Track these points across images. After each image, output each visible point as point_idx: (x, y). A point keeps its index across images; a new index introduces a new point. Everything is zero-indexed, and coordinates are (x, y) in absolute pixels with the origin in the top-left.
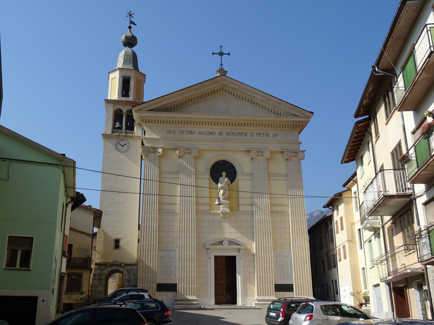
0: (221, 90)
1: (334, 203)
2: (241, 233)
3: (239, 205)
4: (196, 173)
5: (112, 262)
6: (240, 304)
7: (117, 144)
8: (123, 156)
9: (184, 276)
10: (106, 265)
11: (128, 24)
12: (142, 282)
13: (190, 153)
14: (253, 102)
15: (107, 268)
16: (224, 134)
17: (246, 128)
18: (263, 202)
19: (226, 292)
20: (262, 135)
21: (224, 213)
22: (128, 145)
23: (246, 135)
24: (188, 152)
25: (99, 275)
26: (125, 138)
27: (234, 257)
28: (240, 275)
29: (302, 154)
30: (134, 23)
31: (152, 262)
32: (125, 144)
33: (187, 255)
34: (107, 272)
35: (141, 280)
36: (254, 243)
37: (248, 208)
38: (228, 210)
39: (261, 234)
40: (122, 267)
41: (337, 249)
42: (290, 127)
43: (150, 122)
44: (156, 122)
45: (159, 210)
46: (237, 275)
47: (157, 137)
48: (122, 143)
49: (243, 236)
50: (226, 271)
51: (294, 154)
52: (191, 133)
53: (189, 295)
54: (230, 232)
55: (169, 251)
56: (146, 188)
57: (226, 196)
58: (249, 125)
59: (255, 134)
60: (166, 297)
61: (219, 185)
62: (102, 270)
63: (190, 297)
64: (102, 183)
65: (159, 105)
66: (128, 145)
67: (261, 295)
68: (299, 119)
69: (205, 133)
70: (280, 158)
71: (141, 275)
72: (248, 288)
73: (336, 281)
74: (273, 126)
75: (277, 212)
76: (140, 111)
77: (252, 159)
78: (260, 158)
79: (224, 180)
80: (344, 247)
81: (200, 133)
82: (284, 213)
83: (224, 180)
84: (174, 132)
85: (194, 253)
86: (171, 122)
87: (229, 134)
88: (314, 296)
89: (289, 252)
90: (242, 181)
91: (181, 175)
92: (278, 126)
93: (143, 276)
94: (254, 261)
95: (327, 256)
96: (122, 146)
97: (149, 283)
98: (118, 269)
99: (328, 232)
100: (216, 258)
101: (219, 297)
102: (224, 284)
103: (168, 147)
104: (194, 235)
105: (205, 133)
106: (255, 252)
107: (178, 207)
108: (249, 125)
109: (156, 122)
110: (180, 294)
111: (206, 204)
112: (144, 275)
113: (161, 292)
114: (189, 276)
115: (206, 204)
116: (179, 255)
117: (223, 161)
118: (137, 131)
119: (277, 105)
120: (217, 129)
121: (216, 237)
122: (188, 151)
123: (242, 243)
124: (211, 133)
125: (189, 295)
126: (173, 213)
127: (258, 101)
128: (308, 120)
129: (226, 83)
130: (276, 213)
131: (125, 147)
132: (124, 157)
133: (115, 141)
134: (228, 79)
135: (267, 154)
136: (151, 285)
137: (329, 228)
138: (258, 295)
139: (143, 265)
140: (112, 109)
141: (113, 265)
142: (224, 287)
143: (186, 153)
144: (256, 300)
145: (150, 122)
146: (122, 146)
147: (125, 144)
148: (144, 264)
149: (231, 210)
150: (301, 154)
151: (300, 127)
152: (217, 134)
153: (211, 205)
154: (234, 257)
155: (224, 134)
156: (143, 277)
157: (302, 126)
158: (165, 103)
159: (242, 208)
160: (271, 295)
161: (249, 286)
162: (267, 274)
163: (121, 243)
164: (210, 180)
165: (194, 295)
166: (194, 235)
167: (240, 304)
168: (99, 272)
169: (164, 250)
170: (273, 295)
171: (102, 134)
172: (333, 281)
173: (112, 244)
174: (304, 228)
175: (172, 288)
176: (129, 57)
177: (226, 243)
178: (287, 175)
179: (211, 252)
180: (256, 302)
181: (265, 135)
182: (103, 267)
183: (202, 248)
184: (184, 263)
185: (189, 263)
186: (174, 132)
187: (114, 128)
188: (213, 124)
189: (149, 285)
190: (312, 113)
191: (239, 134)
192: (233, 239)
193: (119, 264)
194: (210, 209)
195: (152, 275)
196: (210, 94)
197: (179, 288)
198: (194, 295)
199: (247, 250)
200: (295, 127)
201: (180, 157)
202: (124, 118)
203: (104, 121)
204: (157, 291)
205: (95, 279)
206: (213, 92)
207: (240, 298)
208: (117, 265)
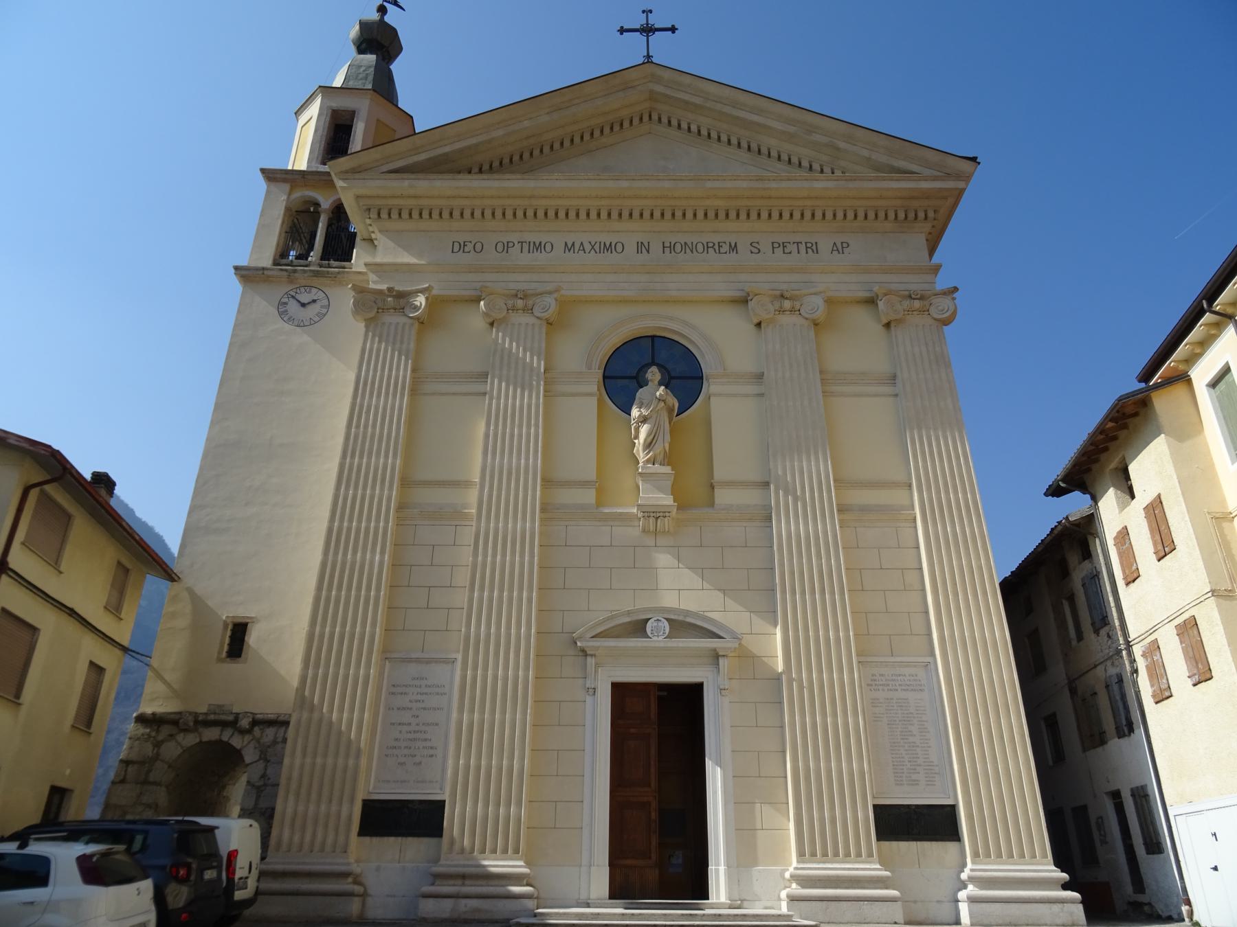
0: (646, 118)
1: (1098, 461)
2: (724, 591)
3: (712, 487)
4: (550, 377)
5: (203, 709)
6: (723, 898)
8: (301, 338)
9: (478, 768)
10: (175, 723)
12: (298, 794)
13: (529, 310)
14: (754, 146)
15: (180, 737)
16: (656, 248)
17: (732, 225)
18: (813, 472)
19: (661, 841)
20: (789, 248)
21: (654, 514)
22: (325, 302)
23: (734, 248)
24: (520, 303)
25: (141, 763)
27: (695, 691)
29: (945, 302)
31: (356, 715)
32: (314, 301)
33: (495, 677)
34: (179, 751)
35: (294, 786)
36: (778, 631)
37: (749, 497)
38: (667, 500)
39: (803, 593)
40: (243, 732)
41: (1137, 650)
42: (891, 215)
43: (395, 215)
44: (415, 214)
45: (401, 507)
47: (413, 260)
48: (305, 298)
52: (539, 247)
53: (494, 851)
54: (678, 587)
55: (428, 661)
56: (358, 427)
57: (659, 448)
59: (765, 247)
60: (387, 867)
62: (158, 745)
63: (496, 865)
65: (423, 157)
66: (325, 302)
67: (814, 854)
68: (925, 185)
69: (588, 247)
71: (298, 762)
73: (1142, 796)
75: (864, 509)
76: (357, 176)
77: (759, 325)
78: (786, 319)
79: (655, 391)
80: (1189, 630)
81: (569, 248)
82: (898, 516)
83: (655, 391)
84: (478, 247)
85: (527, 668)
86: (467, 213)
87: (672, 248)
88: (1060, 862)
89: (927, 665)
90: (726, 408)
91: (494, 385)
92: (850, 215)
93: (335, 766)
94: (781, 703)
95: (1073, 691)
96: (303, 305)
97: (314, 796)
98: (225, 738)
99: (1071, 599)
101: (628, 862)
102: (654, 805)
103: (455, 293)
107: (473, 496)
109: (415, 214)
110: (457, 847)
111: (584, 484)
112: (308, 760)
113: (375, 840)
114: (500, 769)
115: (584, 484)
116: (464, 677)
120: (629, 233)
121: (624, 604)
122: (523, 300)
123: (722, 626)
124: (609, 248)
125: (494, 851)
126: (455, 515)
127: (773, 142)
128: (961, 185)
129: (659, 88)
130: (865, 512)
131: (312, 311)
132: (306, 338)
133: (279, 291)
134: (667, 75)
136: (301, 808)
137: (1079, 574)
138: (801, 854)
140: (284, 197)
141: (208, 724)
145: (395, 215)
146: (303, 305)
147: (314, 301)
148: (316, 715)
150: (941, 306)
151: (930, 215)
152: (631, 248)
153: (601, 487)
154: (695, 691)
155: (656, 248)
158: (447, 149)
159: (723, 497)
161: (764, 814)
162: (820, 672)
163: (253, 638)
165: (516, 851)
167: (723, 898)
168: (149, 750)
169: (410, 660)
170: (870, 855)
171: (236, 268)
172: (1116, 795)
173: (220, 639)
174: (980, 568)
175: (417, 819)
177: (658, 631)
178: (894, 377)
179: (597, 665)
180: (795, 889)
181: (802, 247)
182: (166, 730)
183: (568, 650)
186: (478, 247)
187: (283, 254)
190: (974, 159)
191: (707, 247)
192: (687, 613)
193: (231, 718)
194: (599, 503)
195: (341, 761)
196: (607, 130)
197: (452, 820)
198: (516, 851)
199: (749, 661)
200: (911, 215)
201: (492, 324)
204: (363, 832)
205: (123, 781)
207: (722, 868)
208: (223, 724)
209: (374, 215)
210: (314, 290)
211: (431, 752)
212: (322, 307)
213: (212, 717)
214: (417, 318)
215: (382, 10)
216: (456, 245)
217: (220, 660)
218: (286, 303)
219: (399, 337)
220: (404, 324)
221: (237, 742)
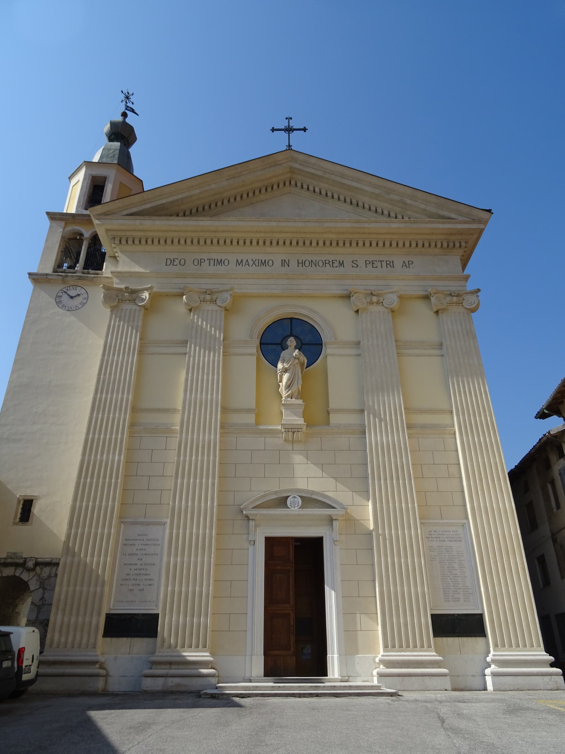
0: (287, 183)
2: (336, 478)
3: (328, 413)
6: (337, 676)
7: (61, 294)
8: (70, 318)
11: (123, 109)
14: (354, 202)
16: (293, 263)
17: (340, 250)
18: (391, 404)
21: (291, 430)
23: (342, 264)
24: (208, 297)
26: (80, 283)
28: (333, 588)
29: (472, 298)
30: (133, 111)
32: (79, 295)
35: (62, 605)
36: (370, 504)
37: (351, 419)
38: (300, 421)
40: (29, 570)
42: (439, 245)
43: (130, 242)
45: (132, 425)
46: (327, 589)
48: (72, 293)
49: (340, 486)
50: (297, 575)
51: (455, 299)
52: (220, 262)
53: (190, 646)
54: (307, 476)
55: (148, 524)
57: (295, 388)
58: (347, 244)
59: (361, 263)
61: (280, 366)
63: (191, 655)
64: (13, 372)
65: (148, 206)
66: (86, 296)
67: (394, 646)
68: (459, 226)
69: (251, 263)
70: (421, 307)
71: (64, 589)
72: (359, 628)
74: (401, 244)
75: (423, 427)
77: (357, 311)
78: (375, 308)
81: (239, 263)
82: (444, 431)
85: (211, 528)
86: (176, 241)
87: (303, 263)
90: (337, 363)
91: (191, 348)
93: (67, 592)
94: (372, 549)
96: (72, 297)
98: (17, 574)
99: (553, 483)
100: (271, 542)
101: (276, 652)
104: (213, 484)
105: (251, 263)
106: (372, 527)
107: (177, 418)
108: (347, 244)
110: (166, 644)
111: (248, 411)
112: (71, 588)
113: (114, 640)
114: (194, 593)
115: (248, 411)
117: (291, 319)
118: (107, 268)
119: (409, 201)
120: (277, 255)
121: (273, 487)
122: (210, 296)
124: (264, 263)
125: (190, 646)
126: (167, 431)
128: (482, 226)
130: (423, 428)
134: (301, 157)
135: (392, 300)
138: (386, 646)
139: (72, 562)
140: (62, 230)
142: (292, 622)
143: (204, 301)
144: (382, 662)
145: (130, 242)
146: (72, 297)
147: (79, 295)
148: (76, 559)
149: (309, 424)
150: (470, 301)
151: (463, 245)
152: (278, 263)
153: (258, 412)
155: (293, 263)
156: (66, 597)
157: (466, 242)
158: (164, 201)
159: (334, 419)
160: (422, 646)
161: (363, 621)
162: (397, 529)
163: (36, 510)
164: (258, 359)
165: (205, 646)
166: (213, 484)
167: (337, 676)
170: (430, 646)
171: (30, 274)
173: (16, 510)
176: (111, 151)
177: (294, 503)
178: (441, 344)
179: (256, 526)
180: (382, 669)
184: (183, 556)
185: (196, 556)
187: (59, 266)
188: (268, 243)
189: (80, 619)
190: (489, 211)
191: (325, 263)
192: (313, 492)
193: (21, 561)
194: (257, 423)
196: (263, 191)
198: (205, 646)
199: (352, 523)
200: (451, 245)
201: (190, 310)
202: (83, 247)
203: (37, 247)
206: (270, 188)
207: (336, 656)
208: (17, 565)
209: (117, 241)
210: (79, 288)
211: (150, 582)
212: (83, 299)
213: (9, 560)
214: (143, 306)
215: (124, 115)
216: (169, 261)
217: (15, 524)
218: (61, 296)
219: (132, 319)
220: (135, 310)
221: (25, 576)
